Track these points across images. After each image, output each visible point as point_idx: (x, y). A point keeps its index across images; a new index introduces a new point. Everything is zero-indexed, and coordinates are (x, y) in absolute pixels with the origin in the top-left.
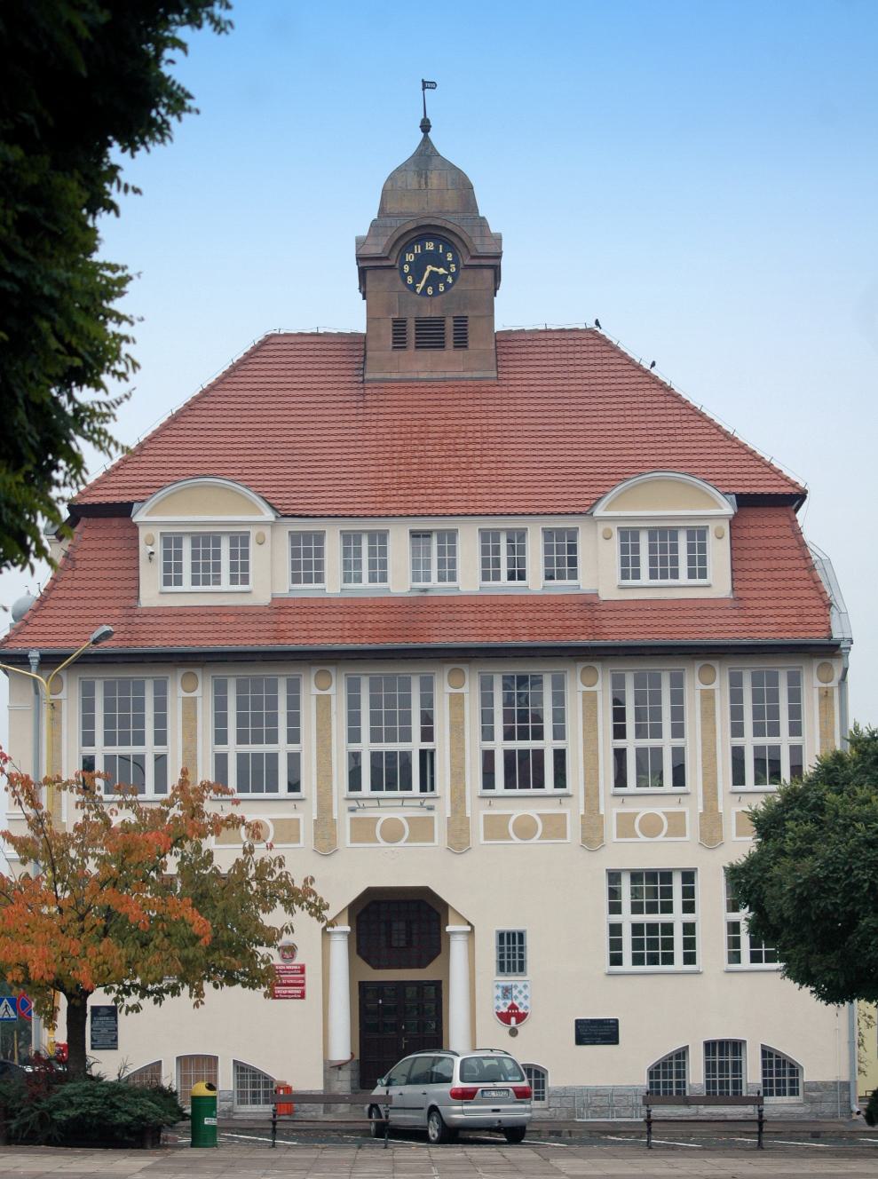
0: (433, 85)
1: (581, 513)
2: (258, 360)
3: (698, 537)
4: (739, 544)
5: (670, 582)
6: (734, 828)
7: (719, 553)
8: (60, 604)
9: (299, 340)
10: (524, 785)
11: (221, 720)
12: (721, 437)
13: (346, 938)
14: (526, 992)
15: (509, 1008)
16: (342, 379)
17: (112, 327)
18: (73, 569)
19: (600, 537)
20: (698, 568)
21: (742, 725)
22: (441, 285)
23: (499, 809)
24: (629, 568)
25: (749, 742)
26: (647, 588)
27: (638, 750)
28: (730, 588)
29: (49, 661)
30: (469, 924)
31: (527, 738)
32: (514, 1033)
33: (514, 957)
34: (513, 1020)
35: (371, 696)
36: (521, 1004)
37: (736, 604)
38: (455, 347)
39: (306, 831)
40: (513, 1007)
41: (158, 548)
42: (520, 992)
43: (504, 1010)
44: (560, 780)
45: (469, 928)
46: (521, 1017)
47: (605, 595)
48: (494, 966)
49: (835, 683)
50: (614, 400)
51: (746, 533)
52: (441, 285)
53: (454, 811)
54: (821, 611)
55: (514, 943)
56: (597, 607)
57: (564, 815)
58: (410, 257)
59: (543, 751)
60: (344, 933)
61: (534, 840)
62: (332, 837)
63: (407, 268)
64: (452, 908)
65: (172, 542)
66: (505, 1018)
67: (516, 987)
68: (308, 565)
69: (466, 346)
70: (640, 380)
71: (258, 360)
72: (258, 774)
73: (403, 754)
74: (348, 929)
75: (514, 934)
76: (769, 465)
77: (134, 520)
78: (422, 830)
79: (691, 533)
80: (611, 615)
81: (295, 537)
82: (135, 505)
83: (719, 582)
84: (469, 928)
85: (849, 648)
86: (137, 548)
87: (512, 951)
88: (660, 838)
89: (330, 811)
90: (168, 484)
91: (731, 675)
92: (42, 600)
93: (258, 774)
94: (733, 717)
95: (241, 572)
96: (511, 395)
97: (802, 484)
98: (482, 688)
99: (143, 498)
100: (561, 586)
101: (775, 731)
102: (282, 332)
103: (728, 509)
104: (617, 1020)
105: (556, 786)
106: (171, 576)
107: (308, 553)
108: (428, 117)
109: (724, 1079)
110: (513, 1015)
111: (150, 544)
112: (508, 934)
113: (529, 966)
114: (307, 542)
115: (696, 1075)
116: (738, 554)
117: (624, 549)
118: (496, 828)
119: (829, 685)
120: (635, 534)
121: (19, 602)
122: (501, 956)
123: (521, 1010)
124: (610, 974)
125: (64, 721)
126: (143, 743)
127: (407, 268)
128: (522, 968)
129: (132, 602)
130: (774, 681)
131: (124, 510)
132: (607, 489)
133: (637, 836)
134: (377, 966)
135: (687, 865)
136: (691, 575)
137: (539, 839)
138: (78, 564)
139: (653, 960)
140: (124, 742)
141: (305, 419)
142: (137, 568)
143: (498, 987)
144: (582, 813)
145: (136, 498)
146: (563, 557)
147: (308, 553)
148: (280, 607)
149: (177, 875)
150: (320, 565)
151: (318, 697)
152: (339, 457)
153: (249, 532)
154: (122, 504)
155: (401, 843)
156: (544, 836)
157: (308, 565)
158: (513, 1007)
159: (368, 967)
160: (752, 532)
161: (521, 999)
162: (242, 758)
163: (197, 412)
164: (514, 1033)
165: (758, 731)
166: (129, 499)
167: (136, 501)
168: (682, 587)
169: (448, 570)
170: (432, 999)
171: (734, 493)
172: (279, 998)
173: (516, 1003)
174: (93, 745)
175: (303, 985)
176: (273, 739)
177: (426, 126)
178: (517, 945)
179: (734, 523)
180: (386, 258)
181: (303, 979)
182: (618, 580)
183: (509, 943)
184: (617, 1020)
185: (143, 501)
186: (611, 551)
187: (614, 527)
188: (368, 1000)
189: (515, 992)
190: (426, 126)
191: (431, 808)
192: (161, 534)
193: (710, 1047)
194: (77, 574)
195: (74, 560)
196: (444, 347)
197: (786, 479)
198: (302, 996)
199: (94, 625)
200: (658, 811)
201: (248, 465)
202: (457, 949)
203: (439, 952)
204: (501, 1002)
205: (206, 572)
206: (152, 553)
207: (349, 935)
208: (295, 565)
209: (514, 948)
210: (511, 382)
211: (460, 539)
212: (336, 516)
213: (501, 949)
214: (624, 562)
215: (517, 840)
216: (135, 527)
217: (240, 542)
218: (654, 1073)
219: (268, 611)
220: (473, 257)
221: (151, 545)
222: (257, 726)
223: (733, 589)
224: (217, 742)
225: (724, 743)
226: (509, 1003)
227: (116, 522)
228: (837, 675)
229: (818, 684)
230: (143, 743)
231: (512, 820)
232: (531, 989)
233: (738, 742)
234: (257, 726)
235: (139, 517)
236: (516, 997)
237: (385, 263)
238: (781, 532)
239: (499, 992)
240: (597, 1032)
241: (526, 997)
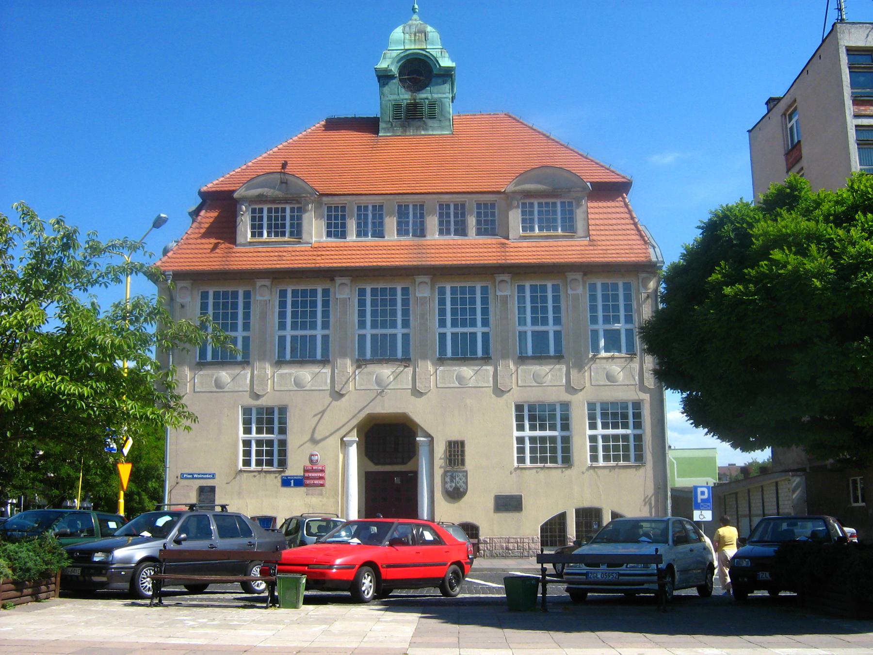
25: (551, 328)
45: (430, 439)
55: (458, 448)
56: (507, 246)
68: (336, 226)
101: (545, 322)
109: (580, 534)
115: (572, 532)
122: (450, 456)
134: (377, 464)
139: (543, 460)
157: (336, 226)
162: (374, 336)
165: (534, 322)
170: (411, 480)
176: (394, 325)
193: (579, 512)
199: (168, 262)
203: (415, 455)
218: (544, 529)
222: (383, 317)
234: (383, 317)
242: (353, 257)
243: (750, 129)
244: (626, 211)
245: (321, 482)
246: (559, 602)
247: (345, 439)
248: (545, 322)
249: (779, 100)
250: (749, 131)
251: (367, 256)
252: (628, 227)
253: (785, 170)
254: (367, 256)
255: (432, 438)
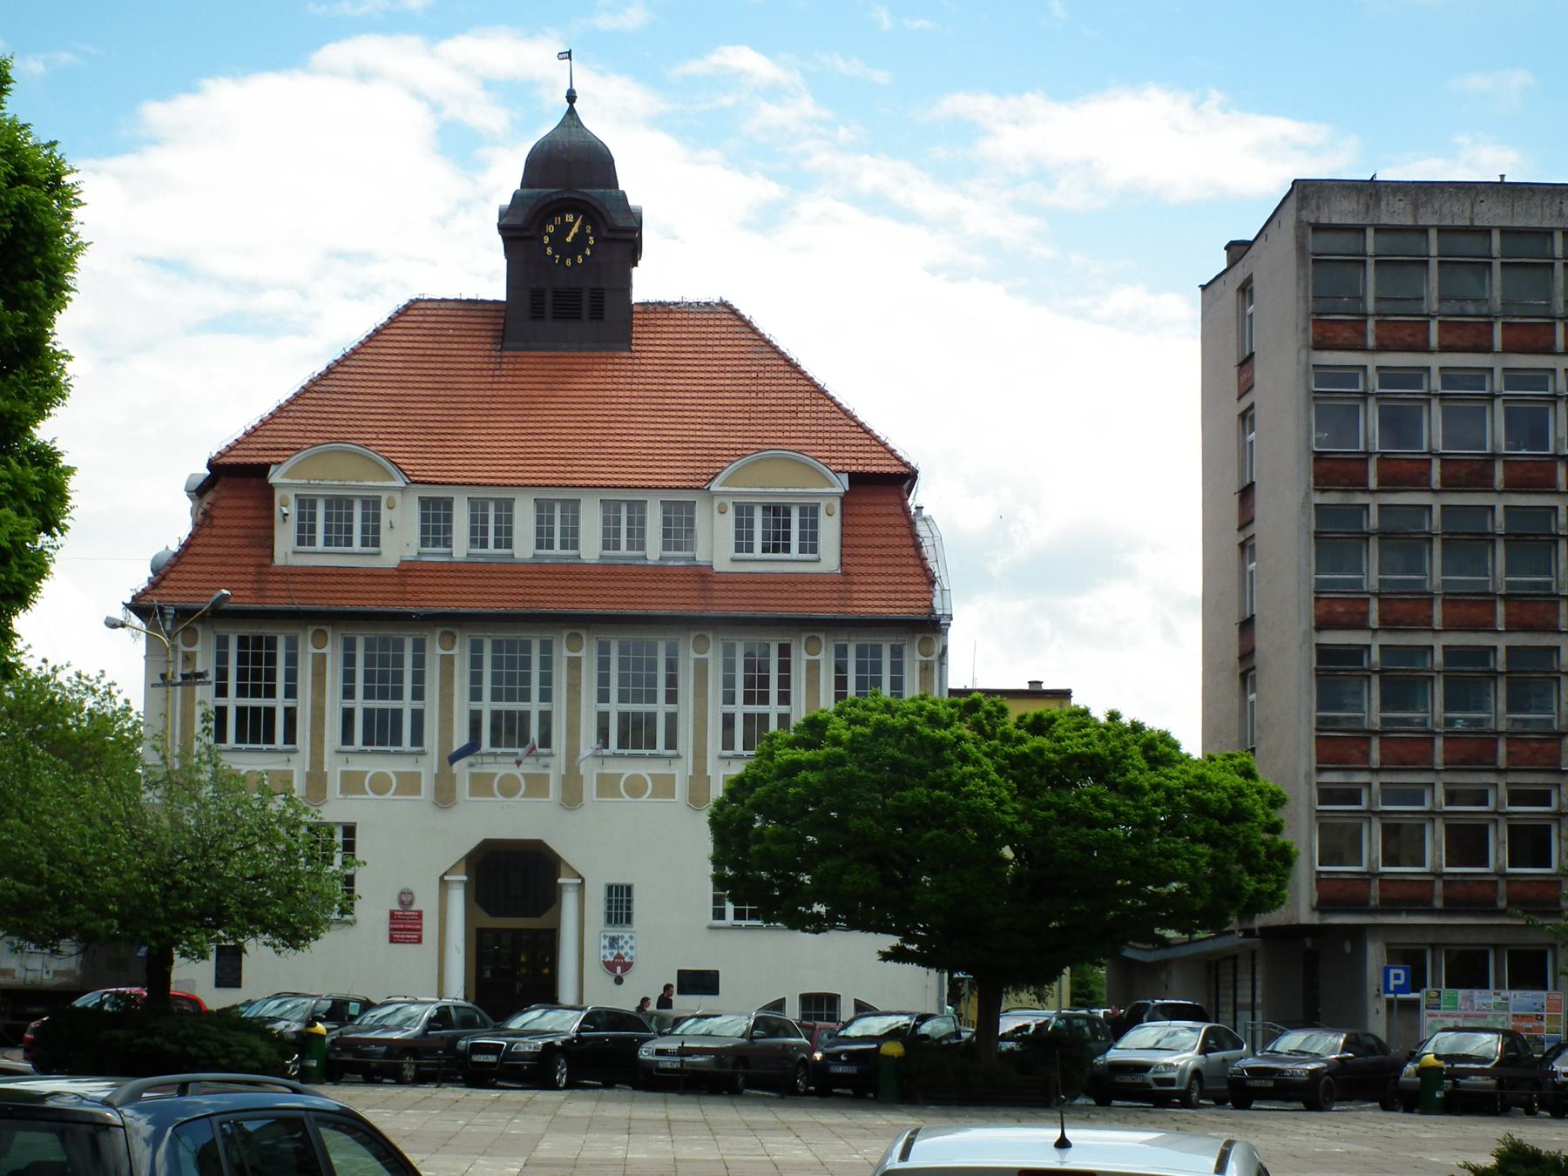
0: (561, 56)
1: (698, 488)
2: (401, 325)
3: (810, 514)
4: (850, 520)
5: (781, 555)
6: (423, 783)
7: (829, 529)
8: (196, 559)
9: (443, 305)
10: (255, 740)
11: (349, 676)
12: (841, 415)
13: (462, 886)
14: (631, 943)
15: (615, 958)
16: (481, 346)
17: (66, 294)
18: (211, 526)
19: (716, 510)
20: (810, 543)
21: (353, 688)
22: (579, 257)
23: (612, 768)
24: (743, 542)
26: (760, 563)
27: (620, 714)
28: (838, 563)
29: (183, 614)
30: (579, 876)
31: (386, 698)
32: (619, 981)
33: (622, 909)
34: (619, 969)
35: (414, 656)
36: (626, 954)
37: (842, 579)
38: (555, 318)
39: (427, 784)
40: (619, 956)
41: (292, 509)
42: (626, 943)
43: (611, 959)
44: (290, 737)
45: (579, 881)
46: (627, 967)
47: (719, 566)
48: (602, 918)
49: (934, 658)
50: (410, 385)
51: (857, 510)
52: (579, 257)
53: (568, 768)
54: (924, 588)
55: (622, 896)
56: (710, 579)
57: (419, 774)
58: (551, 229)
59: (608, 713)
60: (462, 881)
61: (644, 798)
62: (451, 790)
63: (546, 239)
64: (568, 865)
65: (306, 505)
66: (610, 966)
67: (622, 937)
68: (436, 530)
69: (601, 318)
70: (769, 356)
71: (401, 325)
72: (510, 731)
73: (394, 711)
74: (465, 878)
75: (622, 887)
76: (884, 445)
77: (270, 482)
78: (537, 785)
79: (803, 510)
80: (723, 586)
81: (425, 503)
82: (273, 468)
83: (829, 558)
84: (579, 881)
85: (949, 625)
86: (272, 508)
87: (620, 903)
88: (388, 796)
89: (322, 763)
90: (305, 446)
91: (837, 647)
92: (178, 556)
93: (510, 731)
94: (472, 682)
95: (372, 537)
96: (643, 368)
97: (913, 464)
98: (473, 651)
99: (280, 459)
100: (677, 558)
101: (764, 699)
102: (426, 297)
103: (842, 485)
104: (717, 972)
105: (667, 748)
106: (305, 536)
107: (436, 518)
108: (574, 87)
110: (619, 964)
111: (286, 508)
112: (617, 887)
113: (635, 918)
114: (339, 507)
116: (849, 530)
117: (738, 523)
118: (607, 785)
119: (929, 659)
120: (750, 509)
121: (156, 557)
122: (610, 908)
123: (627, 960)
124: (711, 928)
125: (456, 673)
126: (654, 701)
127: (546, 239)
128: (629, 920)
129: (267, 561)
130: (877, 651)
131: (263, 470)
132: (725, 464)
133: (366, 793)
135: (348, 819)
136: (802, 550)
137: (394, 794)
138: (216, 522)
140: (256, 694)
141: (369, 391)
142: (272, 528)
143: (605, 937)
144: (436, 771)
145: (274, 459)
146: (679, 525)
147: (436, 518)
148: (406, 571)
149: (1275, 840)
150: (449, 529)
151: (697, 660)
152: (599, 418)
153: (380, 497)
154: (259, 465)
155: (517, 798)
156: (654, 794)
157: (436, 530)
158: (619, 956)
159: (485, 915)
160: (864, 510)
161: (627, 949)
163: (338, 376)
164: (619, 981)
165: (748, 699)
166: (266, 460)
167: (273, 463)
168: (792, 562)
169: (637, 537)
170: (548, 943)
171: (847, 472)
172: (397, 942)
173: (622, 953)
174: (608, 701)
175: (420, 930)
176: (398, 695)
177: (571, 97)
178: (625, 898)
179: (845, 500)
180: (527, 229)
181: (421, 924)
182: (732, 553)
183: (617, 895)
184: (717, 972)
185: (280, 463)
186: (726, 525)
187: (729, 503)
188: (482, 947)
189: (621, 943)
190: (571, 97)
191: (546, 766)
192: (296, 495)
194: (214, 531)
195: (212, 518)
196: (579, 318)
197: (899, 459)
198: (419, 941)
200: (517, 772)
201: (383, 430)
202: (569, 902)
203: (554, 902)
204: (607, 952)
205: (339, 534)
206: (286, 515)
207: (467, 885)
208: (424, 530)
209: (622, 901)
210: (644, 355)
211: (583, 508)
212: (464, 484)
213: (610, 901)
214: (738, 535)
215: (628, 798)
216: (271, 489)
217: (372, 506)
219: (397, 573)
220: (610, 230)
221: (286, 506)
223: (842, 564)
224: (600, 700)
225: (334, 705)
226: (615, 952)
227: (254, 481)
228: (938, 649)
229: (919, 657)
230: (654, 701)
231: (624, 779)
232: (640, 940)
233: (476, 706)
234: (511, 683)
235: (275, 477)
236: (622, 947)
237: (527, 234)
238: (891, 510)
239: (606, 942)
240: (701, 982)
241: (631, 948)
242: (458, 589)
243: (1205, 283)
244: (905, 522)
245: (418, 927)
246: (843, 1061)
247: (446, 878)
248: (764, 699)
249: (1247, 245)
250: (1203, 288)
251: (486, 590)
252: (905, 551)
253: (1236, 397)
254: (486, 590)
255: (583, 880)
